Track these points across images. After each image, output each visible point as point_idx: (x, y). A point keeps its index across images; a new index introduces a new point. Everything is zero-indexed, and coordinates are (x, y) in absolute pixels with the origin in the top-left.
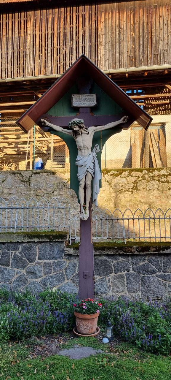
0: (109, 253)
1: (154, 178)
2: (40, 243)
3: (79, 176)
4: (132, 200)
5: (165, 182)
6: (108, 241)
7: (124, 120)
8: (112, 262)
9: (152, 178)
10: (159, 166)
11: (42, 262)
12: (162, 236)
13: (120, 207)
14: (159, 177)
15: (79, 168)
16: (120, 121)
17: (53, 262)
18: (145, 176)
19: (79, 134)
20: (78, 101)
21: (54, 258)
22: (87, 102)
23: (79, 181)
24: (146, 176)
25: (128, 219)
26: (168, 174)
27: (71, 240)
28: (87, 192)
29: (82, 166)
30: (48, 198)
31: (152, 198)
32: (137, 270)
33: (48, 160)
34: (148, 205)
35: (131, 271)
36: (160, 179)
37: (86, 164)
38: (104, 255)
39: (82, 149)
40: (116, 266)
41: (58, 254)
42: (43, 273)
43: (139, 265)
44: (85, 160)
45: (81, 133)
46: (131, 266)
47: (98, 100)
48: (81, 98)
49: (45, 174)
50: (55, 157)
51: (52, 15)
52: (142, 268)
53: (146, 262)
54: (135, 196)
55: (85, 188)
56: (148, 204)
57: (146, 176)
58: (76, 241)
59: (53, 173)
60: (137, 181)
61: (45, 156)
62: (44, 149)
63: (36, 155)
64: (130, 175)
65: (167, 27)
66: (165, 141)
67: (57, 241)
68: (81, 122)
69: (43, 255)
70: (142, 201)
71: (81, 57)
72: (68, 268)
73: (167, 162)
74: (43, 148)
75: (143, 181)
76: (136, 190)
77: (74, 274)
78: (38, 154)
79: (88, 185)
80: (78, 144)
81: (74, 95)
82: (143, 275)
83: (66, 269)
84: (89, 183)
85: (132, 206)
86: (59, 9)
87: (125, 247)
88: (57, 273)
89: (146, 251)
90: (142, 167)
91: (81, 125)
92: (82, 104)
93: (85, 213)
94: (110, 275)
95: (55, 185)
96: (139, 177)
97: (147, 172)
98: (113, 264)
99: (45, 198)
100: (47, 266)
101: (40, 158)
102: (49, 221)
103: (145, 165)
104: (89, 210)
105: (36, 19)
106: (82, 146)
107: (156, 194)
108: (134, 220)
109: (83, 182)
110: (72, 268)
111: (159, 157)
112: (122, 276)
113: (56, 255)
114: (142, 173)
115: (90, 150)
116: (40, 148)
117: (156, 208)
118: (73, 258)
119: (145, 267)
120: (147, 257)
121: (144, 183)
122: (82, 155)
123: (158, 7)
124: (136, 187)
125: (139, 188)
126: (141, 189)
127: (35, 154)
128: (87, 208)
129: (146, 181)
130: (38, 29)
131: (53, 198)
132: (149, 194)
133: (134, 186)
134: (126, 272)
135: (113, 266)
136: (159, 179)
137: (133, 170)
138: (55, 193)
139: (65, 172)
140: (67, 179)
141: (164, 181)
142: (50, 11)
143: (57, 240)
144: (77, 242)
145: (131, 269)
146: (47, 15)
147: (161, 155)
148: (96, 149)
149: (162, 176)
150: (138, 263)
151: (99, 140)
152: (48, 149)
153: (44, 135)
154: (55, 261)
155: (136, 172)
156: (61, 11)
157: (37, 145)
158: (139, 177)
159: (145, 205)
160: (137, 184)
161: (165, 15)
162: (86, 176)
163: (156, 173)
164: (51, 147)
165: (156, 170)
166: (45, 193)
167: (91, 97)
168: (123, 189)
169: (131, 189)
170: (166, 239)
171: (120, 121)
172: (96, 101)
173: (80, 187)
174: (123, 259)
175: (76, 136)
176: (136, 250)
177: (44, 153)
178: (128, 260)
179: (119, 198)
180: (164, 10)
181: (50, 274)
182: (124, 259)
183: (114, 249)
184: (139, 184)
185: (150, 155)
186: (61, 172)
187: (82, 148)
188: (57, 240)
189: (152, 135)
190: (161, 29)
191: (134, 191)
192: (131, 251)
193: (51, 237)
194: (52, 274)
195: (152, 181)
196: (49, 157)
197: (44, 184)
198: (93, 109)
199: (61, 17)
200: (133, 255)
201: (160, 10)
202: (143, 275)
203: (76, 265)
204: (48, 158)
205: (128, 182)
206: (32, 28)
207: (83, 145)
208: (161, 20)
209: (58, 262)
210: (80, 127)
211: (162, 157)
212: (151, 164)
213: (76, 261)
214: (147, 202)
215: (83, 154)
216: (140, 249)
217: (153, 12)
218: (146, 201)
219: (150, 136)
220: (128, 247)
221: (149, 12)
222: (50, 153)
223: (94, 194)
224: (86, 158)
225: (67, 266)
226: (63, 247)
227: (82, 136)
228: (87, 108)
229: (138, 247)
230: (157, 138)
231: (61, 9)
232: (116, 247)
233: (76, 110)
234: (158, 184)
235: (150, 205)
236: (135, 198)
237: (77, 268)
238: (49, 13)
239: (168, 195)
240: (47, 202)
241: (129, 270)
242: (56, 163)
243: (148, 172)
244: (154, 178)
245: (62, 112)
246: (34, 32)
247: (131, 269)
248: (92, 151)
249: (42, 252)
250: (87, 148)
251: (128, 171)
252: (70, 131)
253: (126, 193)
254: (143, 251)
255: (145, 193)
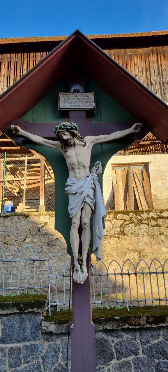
0: (108, 327)
1: (143, 221)
2: (5, 317)
3: (70, 211)
4: (119, 248)
5: (155, 226)
6: (102, 306)
7: (136, 128)
8: (113, 341)
9: (141, 222)
10: (145, 207)
11: (6, 348)
12: (109, 276)
13: (104, 256)
14: (148, 221)
15: (71, 198)
16: (131, 130)
17: (24, 346)
18: (132, 219)
19: (71, 145)
20: (66, 101)
21: (25, 339)
22: (81, 104)
23: (71, 218)
24: (134, 219)
25: (129, 275)
26: (158, 216)
27: (51, 306)
28: (84, 233)
29: (76, 193)
30: (19, 246)
31: (141, 245)
32: (149, 352)
33: (19, 204)
34: (137, 253)
35: (141, 355)
36: (150, 223)
37: (82, 190)
38: (101, 331)
39: (75, 167)
40: (118, 347)
41: (32, 333)
42: (7, 365)
43: (151, 343)
44: (80, 185)
45: (74, 145)
46: (141, 346)
47: (97, 101)
48: (72, 97)
49: (15, 218)
50: (29, 200)
51: (28, 58)
52: (156, 349)
53: (161, 338)
54: (122, 242)
55: (81, 230)
56: (138, 252)
57: (134, 219)
58: (57, 308)
59: (26, 216)
60: (124, 225)
61: (16, 199)
62: (15, 191)
63: (6, 198)
64: (115, 218)
65: (142, 74)
66: (150, 181)
67: (31, 312)
68: (74, 126)
69: (9, 336)
70: (131, 248)
71: (73, 35)
72: (46, 355)
73: (154, 204)
74: (14, 190)
75: (130, 225)
76: (122, 236)
77: (56, 365)
78: (8, 196)
79: (85, 224)
80: (68, 161)
81: (62, 93)
82: (158, 361)
83: (43, 357)
84: (87, 220)
85: (119, 254)
86: (35, 53)
87: (130, 317)
88: (29, 364)
89: (161, 323)
90: (126, 209)
91: (75, 131)
92: (73, 106)
93: (82, 271)
94: (110, 362)
95: (27, 231)
96: (125, 221)
97: (134, 215)
98: (113, 345)
99: (15, 247)
100: (14, 354)
101: (10, 201)
102: (19, 276)
103: (130, 207)
104: (86, 266)
105: (11, 61)
106: (76, 163)
107: (146, 240)
108: (136, 275)
109: (77, 219)
110: (53, 354)
111: (144, 199)
112: (127, 364)
113: (28, 334)
114: (129, 216)
115: (88, 169)
116: (10, 190)
117: (147, 256)
118: (54, 338)
119: (160, 347)
120: (162, 331)
121: (131, 227)
122: (76, 177)
123: (132, 56)
124: (123, 231)
125: (126, 233)
126: (129, 234)
127: (5, 197)
128: (85, 263)
129: (134, 225)
130: (12, 71)
131: (25, 246)
132: (138, 240)
133: (120, 231)
134: (133, 356)
135: (113, 348)
136: (148, 222)
137: (118, 213)
138: (28, 240)
139: (40, 215)
140: (42, 224)
141: (154, 225)
142: (26, 54)
143: (30, 310)
144: (59, 310)
145: (140, 351)
146: (22, 58)
147: (146, 197)
148: (97, 168)
149: (151, 218)
150: (149, 342)
151: (100, 155)
152: (20, 191)
153: (16, 176)
154: (27, 344)
155: (122, 215)
156: (37, 55)
157: (7, 186)
158: (125, 221)
159: (134, 252)
160: (124, 228)
161: (140, 63)
162: (82, 209)
163: (145, 215)
164: (23, 189)
165: (144, 213)
166: (15, 241)
167: (86, 97)
168: (108, 234)
169: (118, 234)
170: (109, 276)
171: (131, 130)
172: (94, 102)
173: (72, 227)
174: (127, 336)
175: (65, 148)
176: (147, 322)
177: (15, 196)
178: (135, 336)
179: (104, 245)
180: (138, 59)
181: (19, 366)
182: (129, 336)
183: (115, 321)
184: (126, 229)
185: (134, 195)
186: (35, 216)
187: (75, 166)
188: (30, 310)
189: (135, 175)
190: (137, 76)
191: (120, 236)
192: (140, 323)
193: (22, 306)
194: (22, 366)
195: (141, 225)
196: (21, 200)
197: (15, 230)
198: (89, 113)
199: (37, 61)
200: (142, 329)
201: (135, 59)
202: (158, 361)
203: (59, 348)
204: (20, 201)
205: (114, 227)
206: (6, 69)
207: (78, 161)
208: (136, 67)
209: (32, 345)
210: (73, 135)
211: (147, 199)
212: (136, 206)
213: (58, 342)
214: (136, 249)
215: (78, 175)
216: (151, 319)
217: (128, 60)
218: (135, 248)
219: (133, 176)
220: (134, 317)
221: (124, 60)
222: (23, 196)
223: (96, 238)
224: (80, 182)
225: (44, 352)
226: (39, 321)
227: (75, 148)
228: (81, 112)
229: (149, 317)
230: (140, 178)
231: (37, 53)
232: (117, 318)
233: (65, 114)
234: (148, 228)
235: (140, 253)
236: (122, 245)
237: (61, 353)
238: (24, 56)
239: (159, 240)
240: (16, 252)
241: (137, 353)
242: (28, 207)
243: (135, 214)
244: (143, 221)
245: (43, 117)
246: (8, 73)
247: (140, 351)
248: (91, 172)
249: (8, 330)
250: (84, 166)
251: (113, 214)
252: (57, 142)
253: (111, 238)
254: (156, 323)
255: (134, 239)
